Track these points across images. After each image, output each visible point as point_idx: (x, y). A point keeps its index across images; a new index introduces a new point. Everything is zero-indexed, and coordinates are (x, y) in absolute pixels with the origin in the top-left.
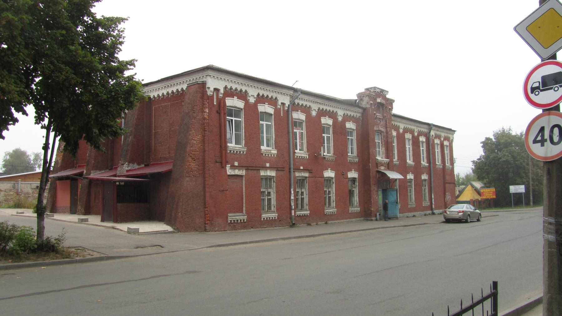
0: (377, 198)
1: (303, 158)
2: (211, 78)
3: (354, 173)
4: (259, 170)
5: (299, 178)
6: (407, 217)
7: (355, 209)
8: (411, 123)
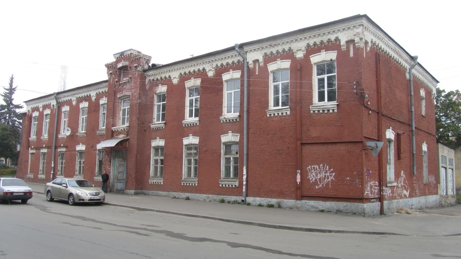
0: (109, 169)
1: (321, 111)
2: (341, 32)
3: (82, 146)
4: (39, 150)
5: (63, 152)
6: (175, 198)
7: (98, 178)
8: (80, 91)
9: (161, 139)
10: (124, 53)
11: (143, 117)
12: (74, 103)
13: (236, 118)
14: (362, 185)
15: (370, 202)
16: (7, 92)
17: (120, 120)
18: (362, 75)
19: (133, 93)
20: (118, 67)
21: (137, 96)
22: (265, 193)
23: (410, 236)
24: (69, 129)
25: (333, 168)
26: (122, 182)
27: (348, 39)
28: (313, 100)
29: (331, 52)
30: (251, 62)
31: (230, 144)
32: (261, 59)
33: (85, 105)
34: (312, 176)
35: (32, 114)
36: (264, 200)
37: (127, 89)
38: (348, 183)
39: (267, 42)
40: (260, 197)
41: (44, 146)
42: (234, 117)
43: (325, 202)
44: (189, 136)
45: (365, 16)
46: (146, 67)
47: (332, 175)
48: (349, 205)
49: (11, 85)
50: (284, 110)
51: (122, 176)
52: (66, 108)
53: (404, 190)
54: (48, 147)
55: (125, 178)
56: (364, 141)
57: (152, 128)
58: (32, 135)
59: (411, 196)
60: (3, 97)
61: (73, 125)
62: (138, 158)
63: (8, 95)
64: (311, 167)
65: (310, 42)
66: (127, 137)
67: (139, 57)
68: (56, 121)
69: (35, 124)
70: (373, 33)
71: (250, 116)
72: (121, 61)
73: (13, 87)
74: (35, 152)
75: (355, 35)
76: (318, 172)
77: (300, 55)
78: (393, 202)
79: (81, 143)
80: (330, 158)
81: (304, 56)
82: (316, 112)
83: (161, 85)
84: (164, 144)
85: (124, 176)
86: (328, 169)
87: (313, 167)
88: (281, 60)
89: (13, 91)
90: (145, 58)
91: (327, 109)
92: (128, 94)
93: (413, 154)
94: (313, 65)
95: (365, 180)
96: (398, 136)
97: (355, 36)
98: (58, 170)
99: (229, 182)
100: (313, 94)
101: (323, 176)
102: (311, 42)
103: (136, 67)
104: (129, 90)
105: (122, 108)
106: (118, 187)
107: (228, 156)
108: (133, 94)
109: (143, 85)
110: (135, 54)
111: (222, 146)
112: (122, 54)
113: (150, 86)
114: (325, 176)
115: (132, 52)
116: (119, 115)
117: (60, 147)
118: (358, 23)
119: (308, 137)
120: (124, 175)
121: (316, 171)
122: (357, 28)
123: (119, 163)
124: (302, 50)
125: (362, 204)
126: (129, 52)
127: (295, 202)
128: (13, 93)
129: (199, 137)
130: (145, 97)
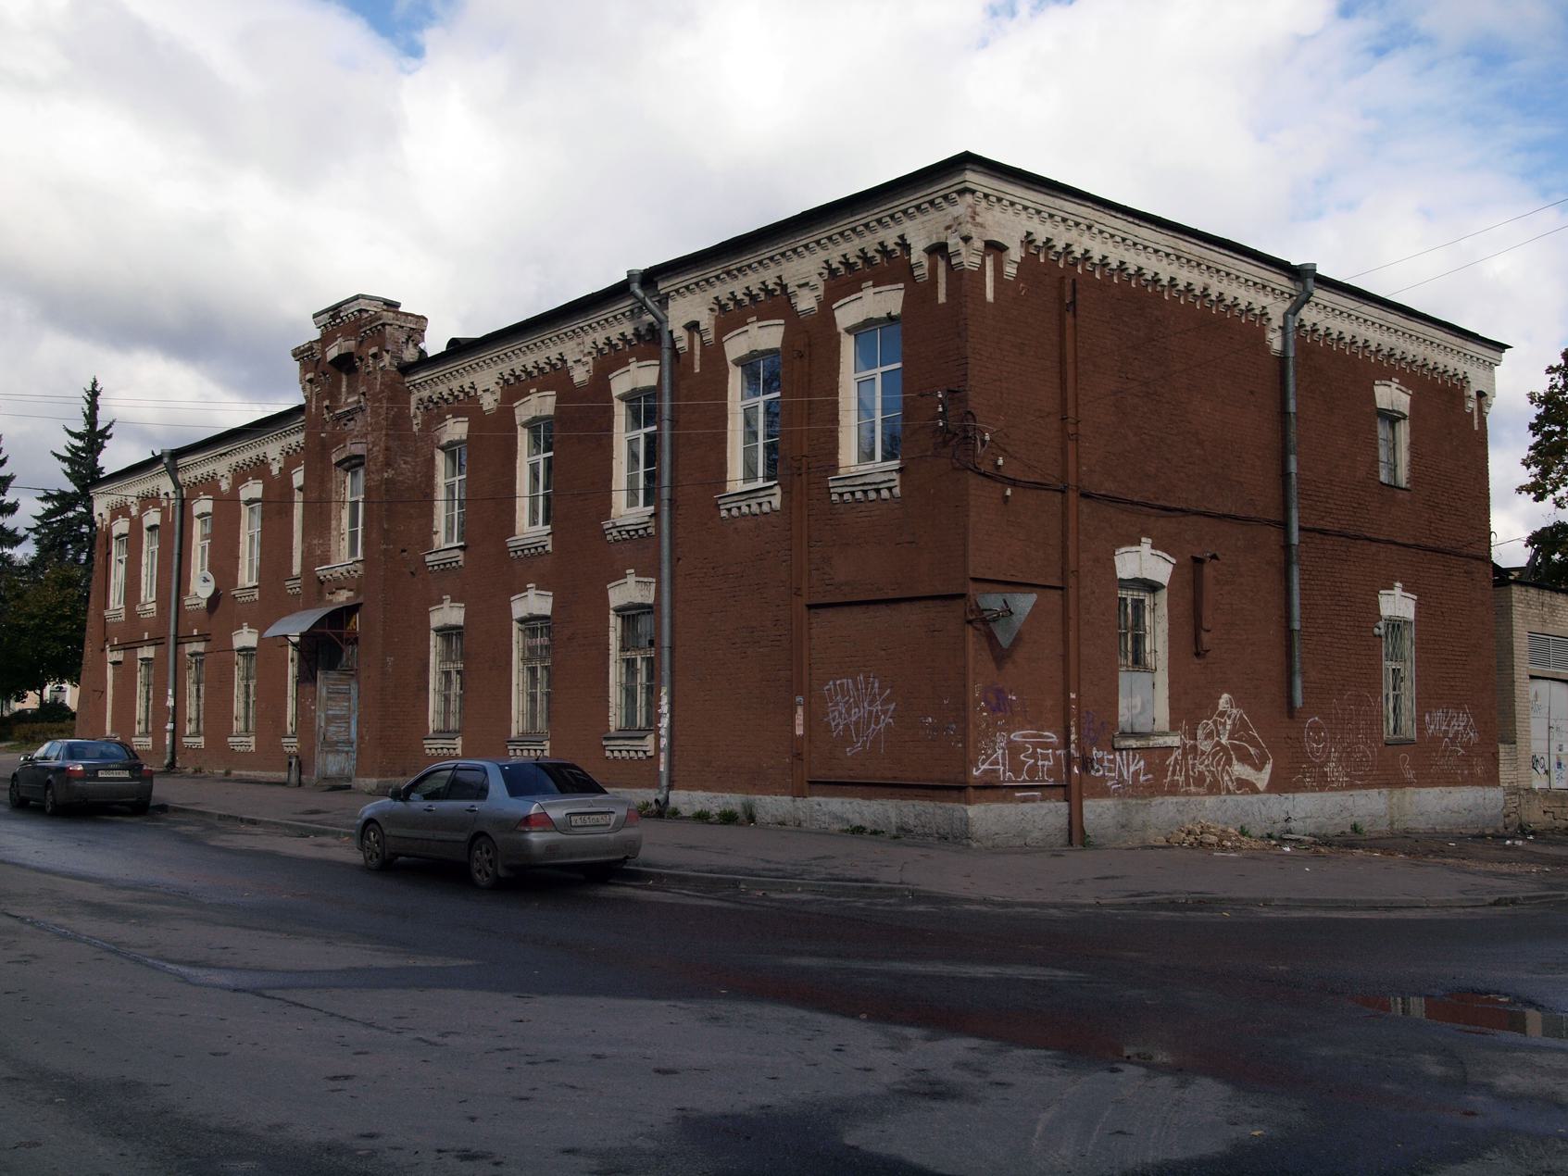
0: (313, 707)
9: (455, 602)
10: (340, 311)
11: (402, 528)
12: (225, 486)
13: (645, 525)
14: (965, 741)
15: (1004, 799)
16: (79, 443)
17: (343, 539)
18: (969, 366)
19: (370, 446)
20: (329, 359)
21: (381, 458)
22: (719, 775)
23: (325, 812)
24: (210, 577)
25: (891, 687)
26: (343, 752)
27: (931, 241)
28: (840, 457)
29: (888, 287)
30: (679, 332)
31: (634, 612)
32: (706, 321)
33: (253, 489)
34: (836, 713)
35: (111, 527)
36: (715, 797)
37: (356, 433)
38: (929, 735)
39: (718, 259)
40: (706, 789)
41: (195, 632)
42: (639, 522)
43: (867, 802)
44: (526, 590)
45: (966, 160)
46: (410, 355)
47: (888, 709)
48: (931, 810)
49: (91, 417)
50: (762, 493)
51: (343, 729)
52: (203, 505)
53: (1235, 762)
54: (157, 641)
55: (354, 736)
56: (971, 592)
57: (431, 564)
58: (114, 601)
59: (1277, 786)
60: (66, 466)
61: (224, 562)
62: (390, 670)
63: (84, 455)
64: (835, 685)
65: (832, 256)
66: (358, 597)
67: (381, 322)
68: (176, 551)
69: (120, 561)
70: (703, 283)
71: (679, 517)
72: (336, 339)
73: (100, 427)
74: (121, 659)
75: (948, 228)
76: (852, 700)
77: (806, 302)
78: (1153, 804)
79: (246, 624)
80: (883, 652)
81: (819, 303)
82: (846, 497)
83: (453, 417)
84: (463, 619)
85: (349, 732)
86: (877, 690)
87: (842, 684)
88: (758, 320)
89: (100, 440)
90: (403, 324)
91: (874, 487)
92: (358, 449)
93: (1291, 631)
94: (842, 335)
95: (977, 726)
96: (1192, 572)
97: (950, 231)
98: (188, 717)
99: (626, 742)
100: (840, 435)
101: (864, 713)
102: (835, 255)
103: (375, 356)
104: (361, 437)
105: (349, 498)
106: (330, 767)
107: (629, 655)
108: (371, 450)
109: (399, 421)
110: (375, 309)
111: (615, 622)
112: (335, 310)
113: (423, 421)
114: (870, 712)
115: (363, 304)
116: (339, 525)
117: (191, 639)
118: (953, 183)
119: (827, 582)
120: (349, 727)
121: (847, 698)
122: (954, 203)
123: (328, 688)
124: (811, 284)
125: (963, 806)
126: (352, 307)
127: (791, 804)
128: (102, 447)
129: (551, 594)
130: (409, 459)
